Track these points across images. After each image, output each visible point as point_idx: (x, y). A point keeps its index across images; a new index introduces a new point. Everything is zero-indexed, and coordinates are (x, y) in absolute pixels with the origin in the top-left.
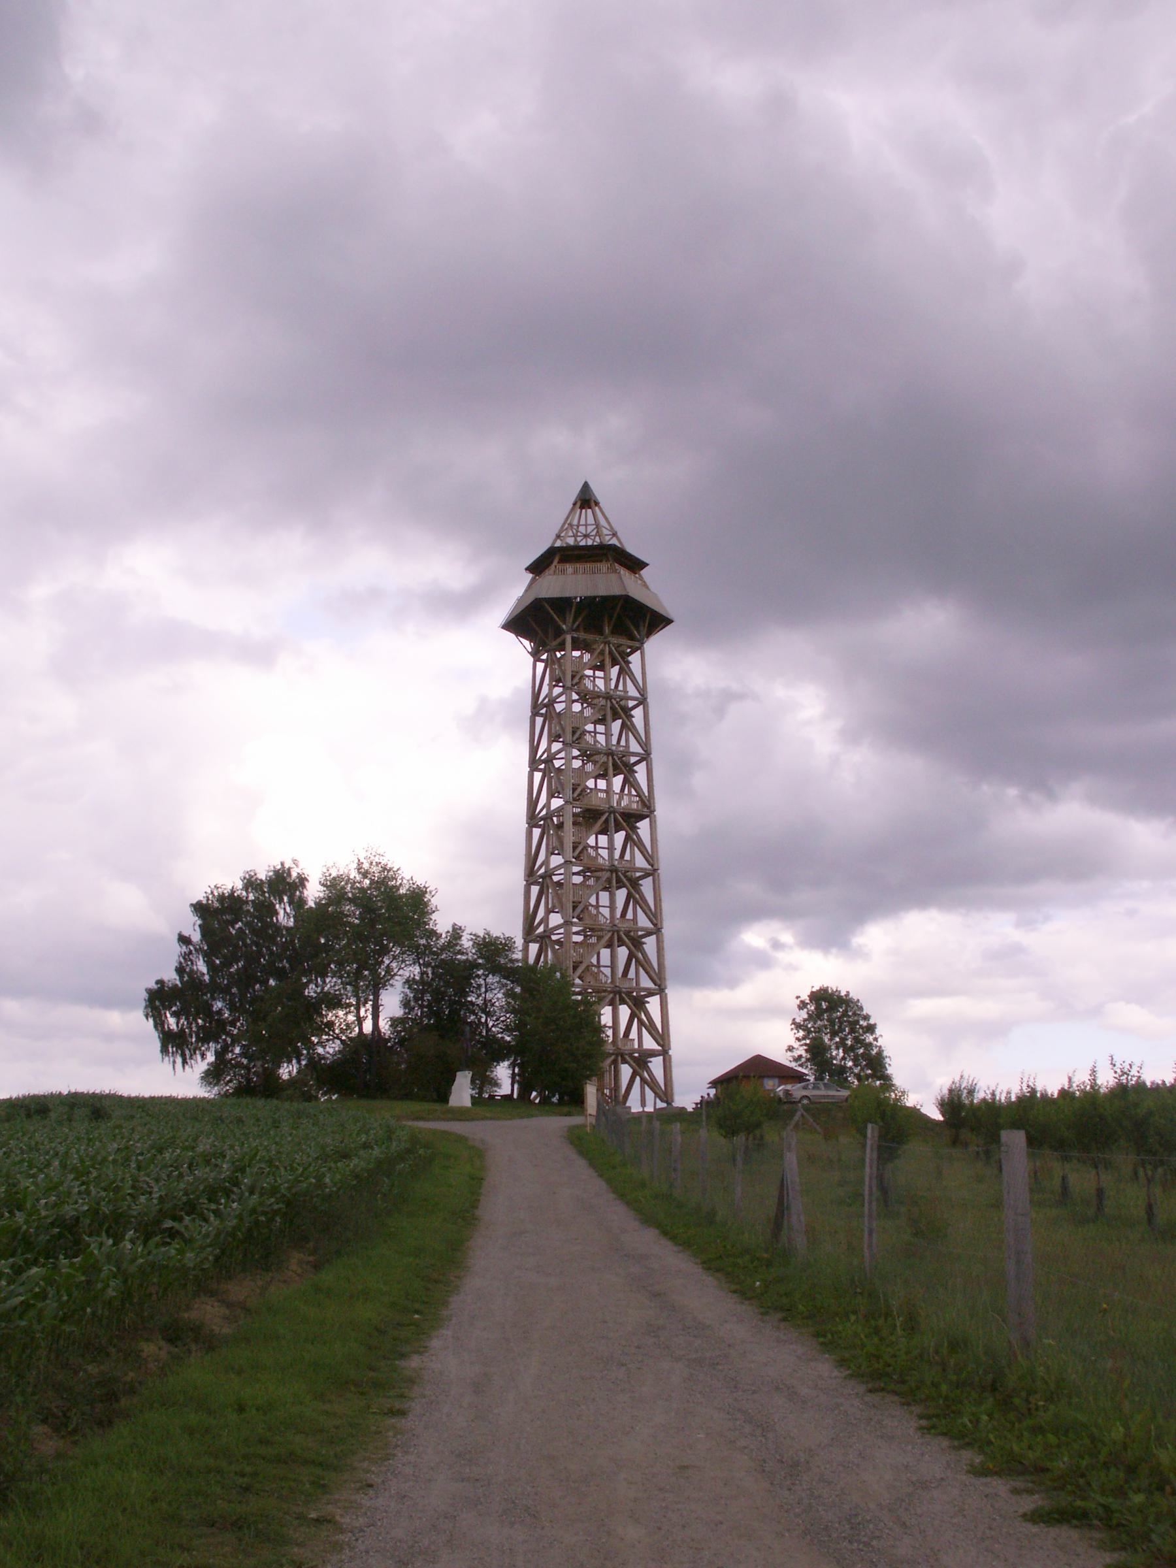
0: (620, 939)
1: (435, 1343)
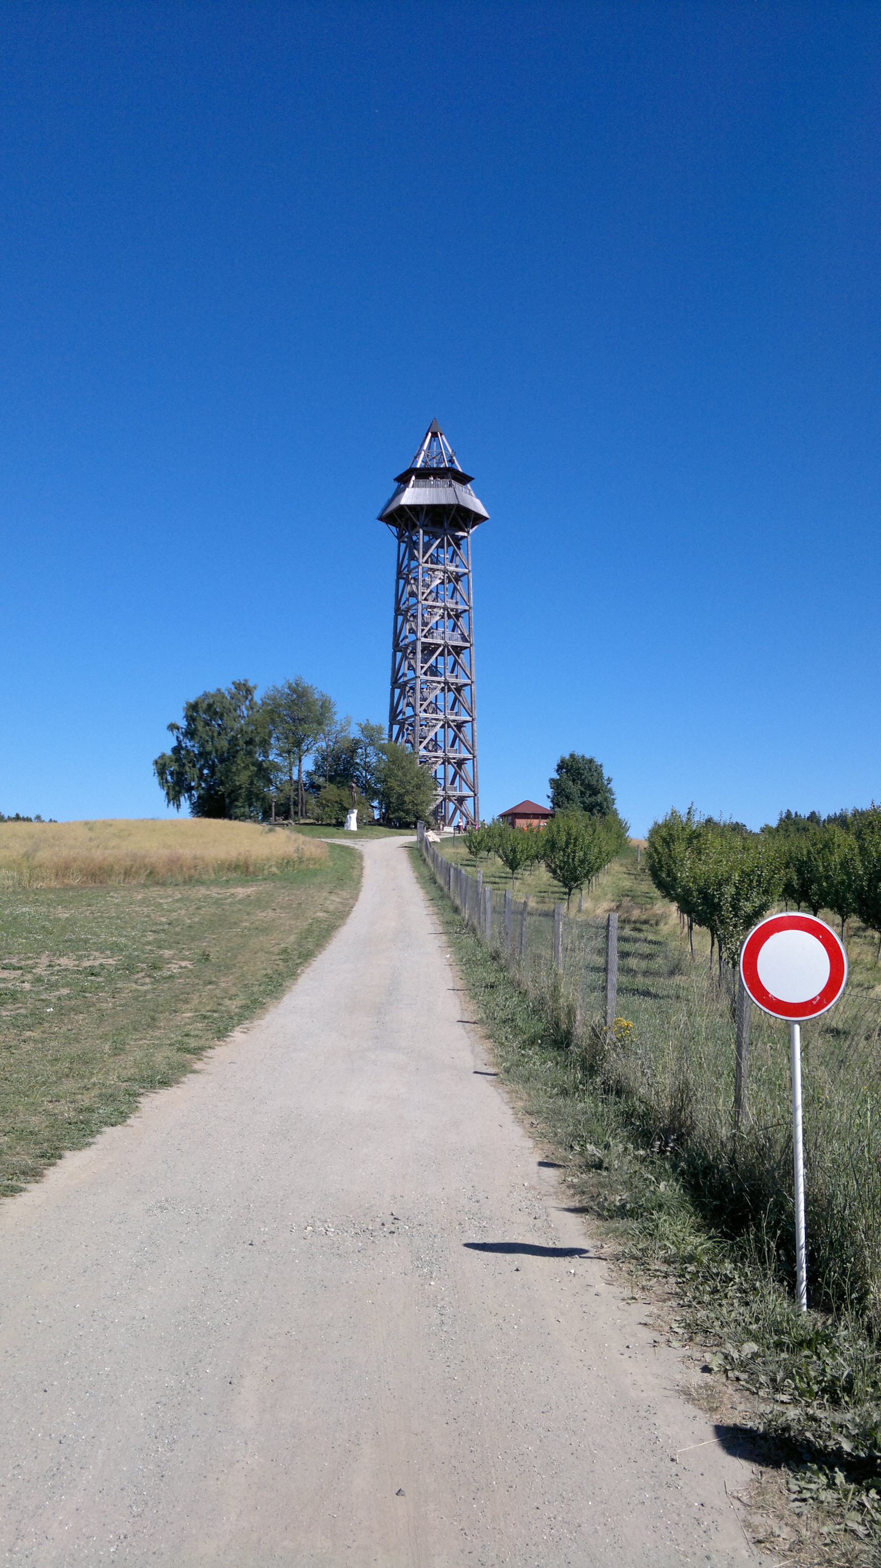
0: (449, 651)
1: (284, 999)
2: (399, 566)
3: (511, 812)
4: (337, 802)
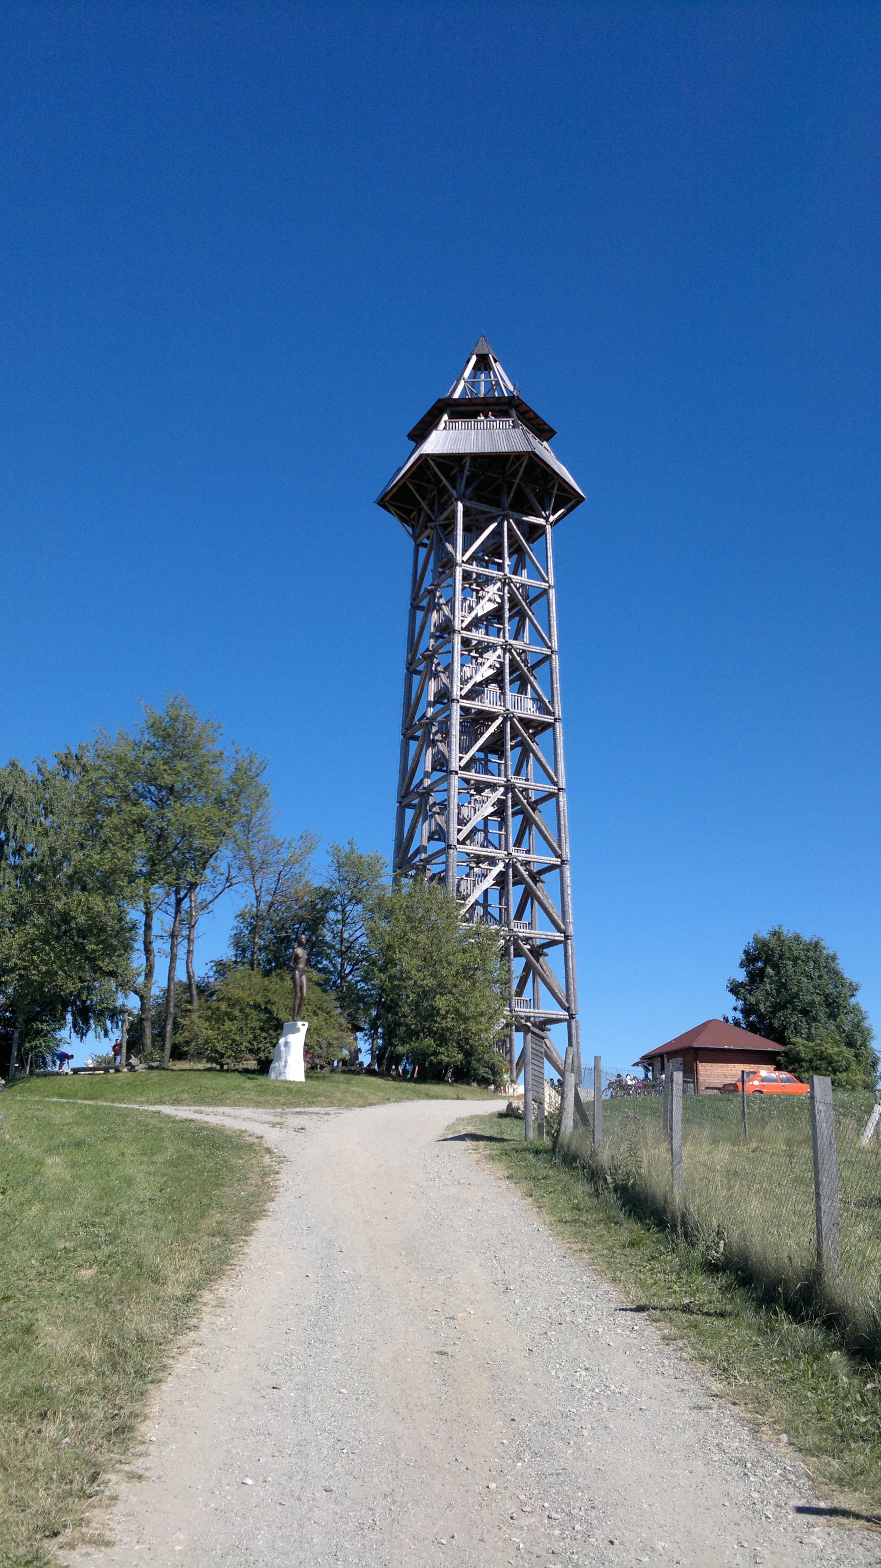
2: (417, 583)
3: (680, 1046)
4: (257, 1006)
